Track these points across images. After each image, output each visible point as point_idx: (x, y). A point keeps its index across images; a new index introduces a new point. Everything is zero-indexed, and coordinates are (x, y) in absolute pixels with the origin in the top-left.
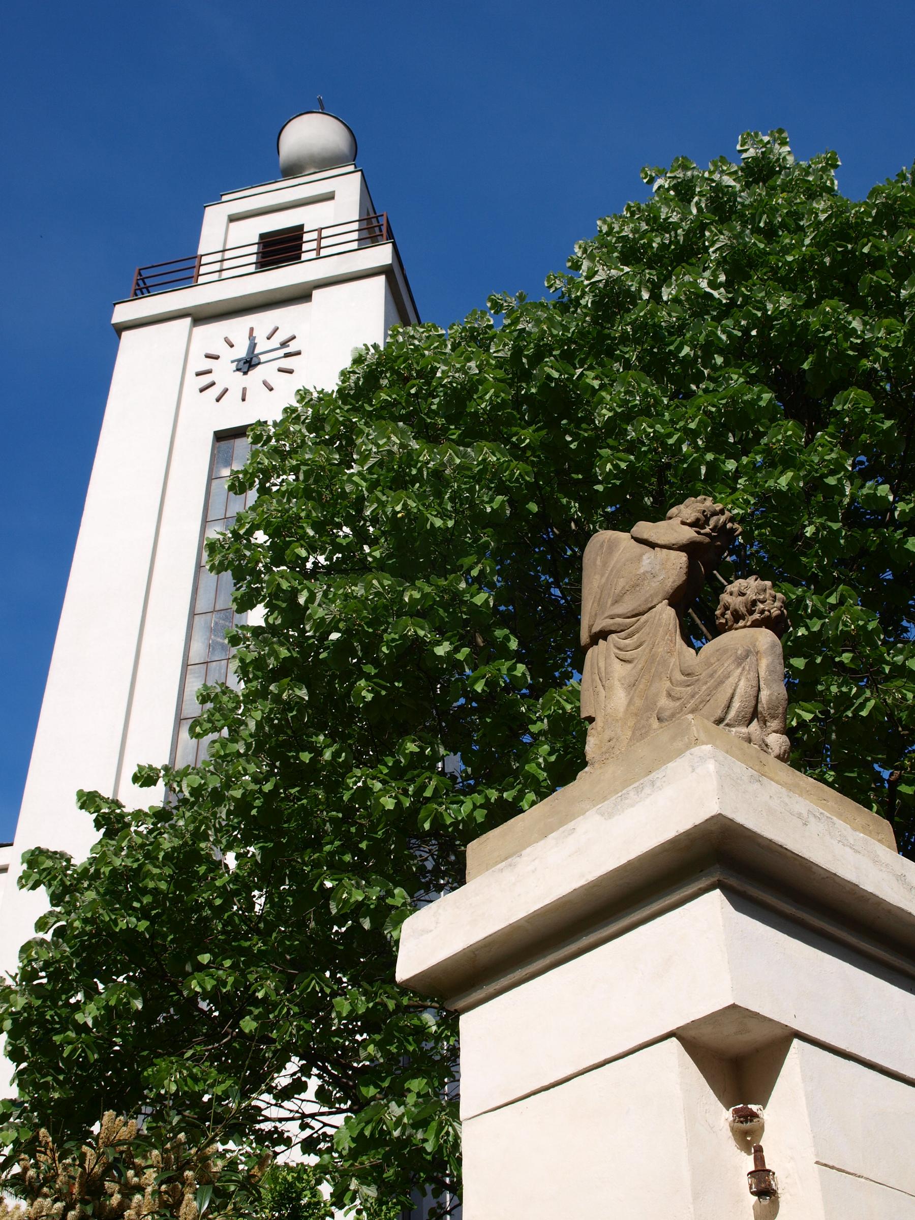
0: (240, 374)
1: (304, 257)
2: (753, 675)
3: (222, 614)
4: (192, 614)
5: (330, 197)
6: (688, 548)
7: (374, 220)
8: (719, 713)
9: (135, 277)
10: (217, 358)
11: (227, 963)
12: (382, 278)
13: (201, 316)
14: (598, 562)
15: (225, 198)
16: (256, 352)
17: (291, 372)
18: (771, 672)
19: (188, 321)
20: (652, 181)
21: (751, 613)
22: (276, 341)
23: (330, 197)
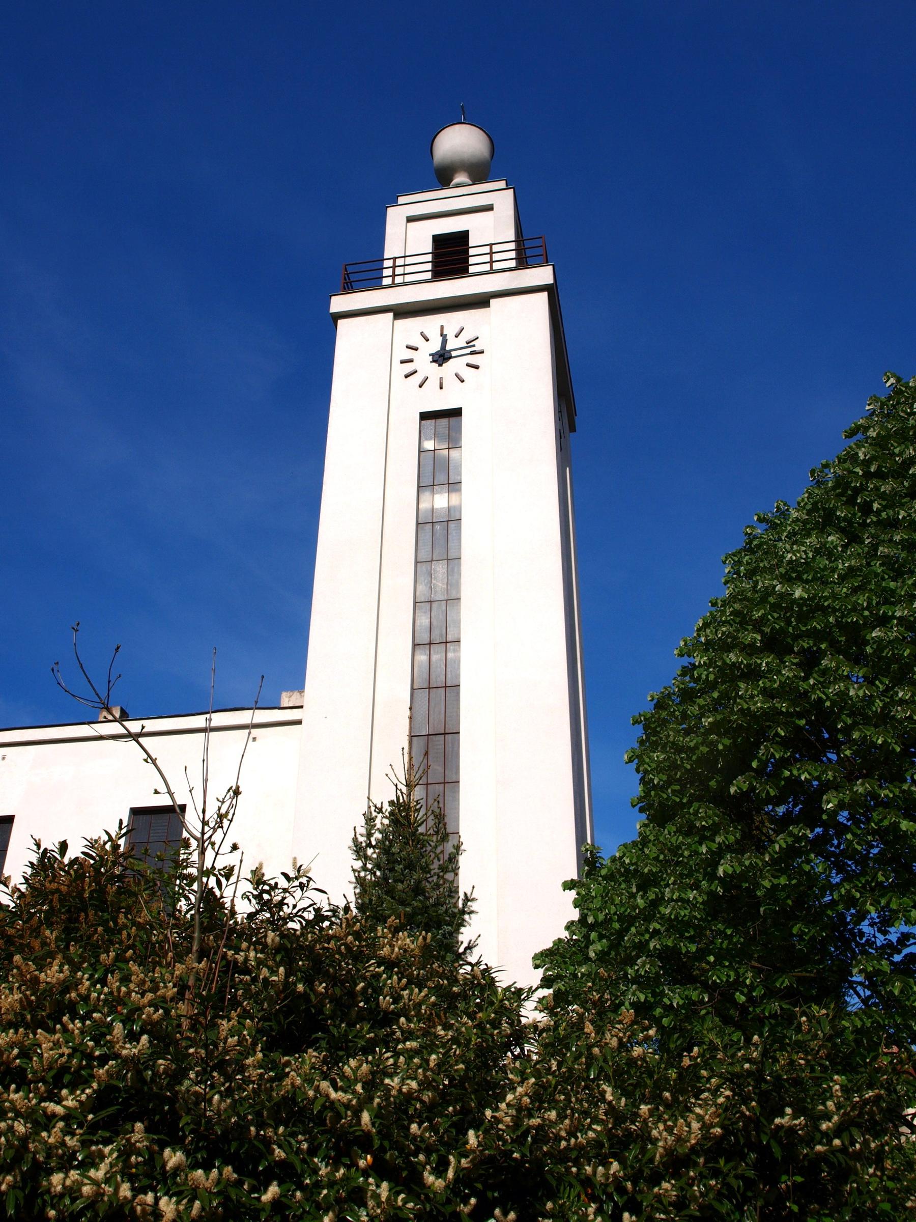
0: (435, 365)
5: (490, 208)
10: (416, 349)
13: (402, 312)
15: (401, 200)
16: (448, 348)
17: (477, 367)
19: (391, 315)
22: (461, 342)
23: (490, 208)
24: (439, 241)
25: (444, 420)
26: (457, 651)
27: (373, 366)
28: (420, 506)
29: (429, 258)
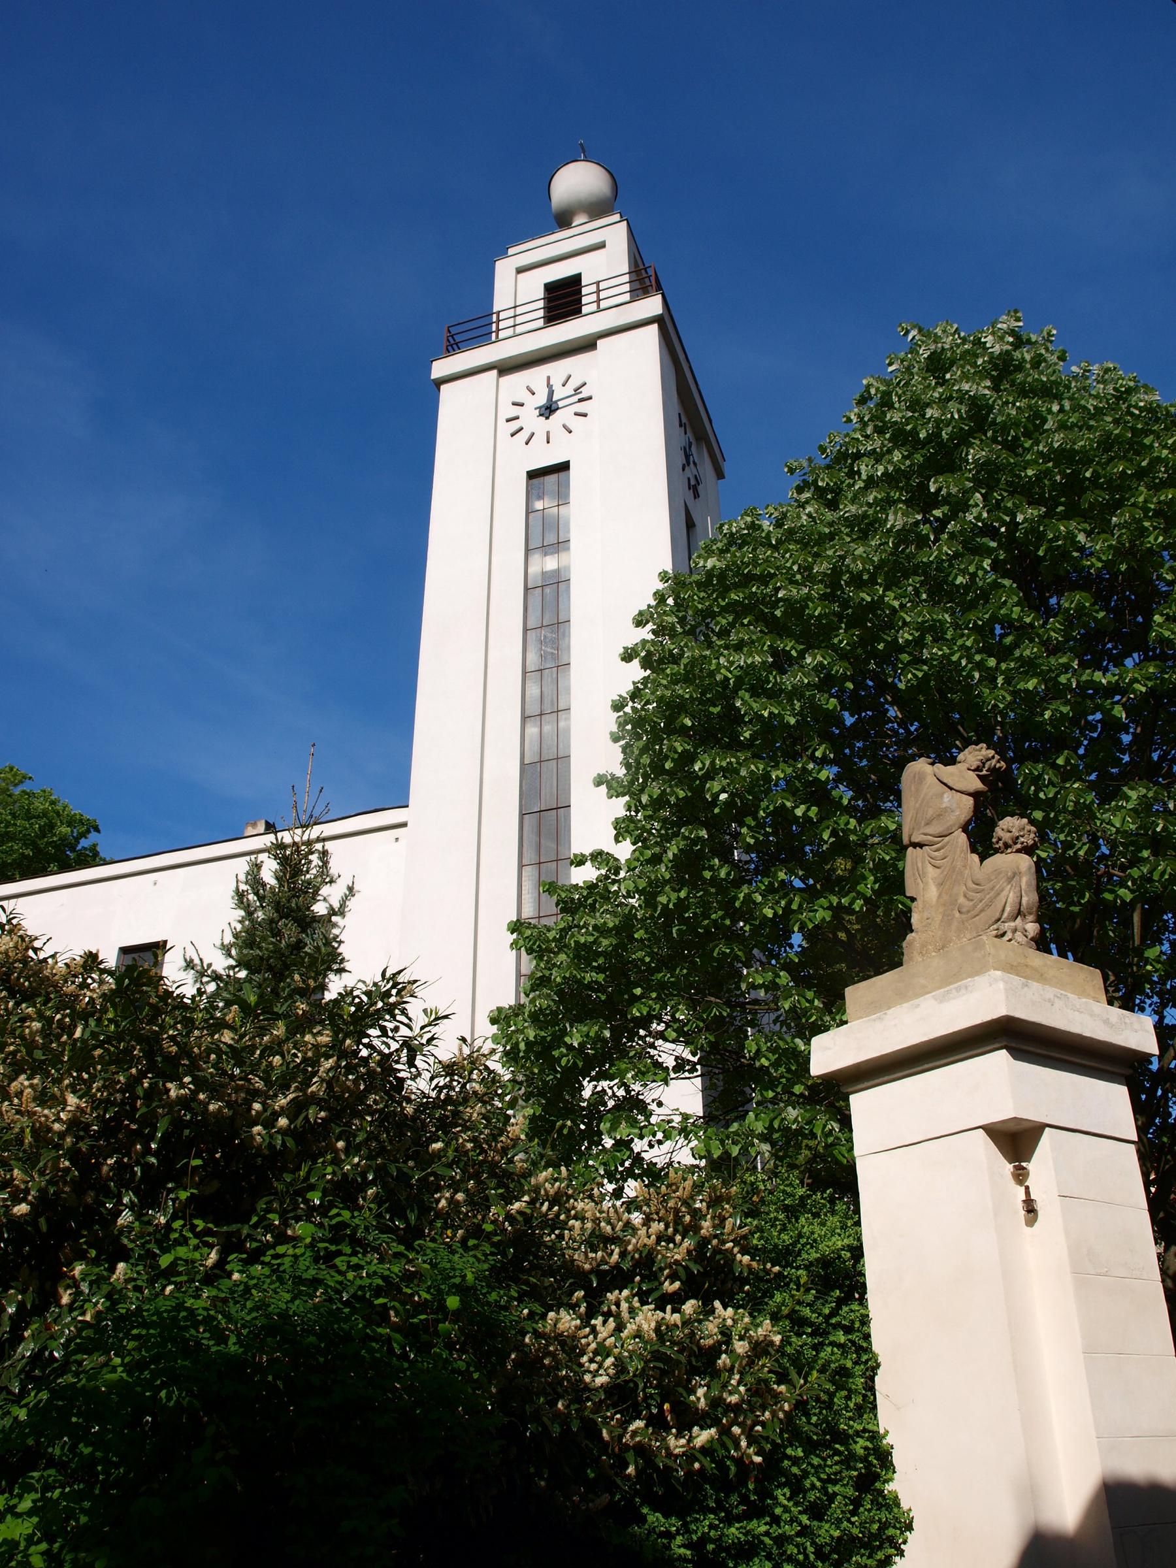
1: (585, 310)
2: (1018, 889)
3: (548, 629)
4: (526, 630)
5: (601, 246)
6: (975, 795)
7: (647, 280)
8: (997, 915)
9: (446, 334)
10: (522, 405)
11: (654, 995)
12: (655, 326)
13: (505, 368)
14: (913, 788)
15: (511, 251)
17: (585, 415)
18: (1028, 885)
19: (495, 372)
20: (907, 332)
21: (1015, 843)
22: (569, 389)
23: (601, 246)
24: (550, 288)
25: (549, 477)
26: (568, 719)
27: (476, 429)
28: (530, 571)
29: (541, 304)
